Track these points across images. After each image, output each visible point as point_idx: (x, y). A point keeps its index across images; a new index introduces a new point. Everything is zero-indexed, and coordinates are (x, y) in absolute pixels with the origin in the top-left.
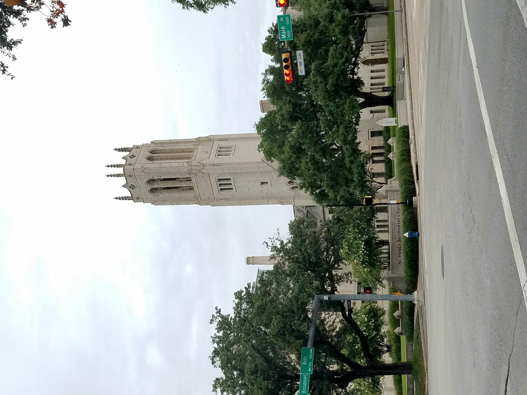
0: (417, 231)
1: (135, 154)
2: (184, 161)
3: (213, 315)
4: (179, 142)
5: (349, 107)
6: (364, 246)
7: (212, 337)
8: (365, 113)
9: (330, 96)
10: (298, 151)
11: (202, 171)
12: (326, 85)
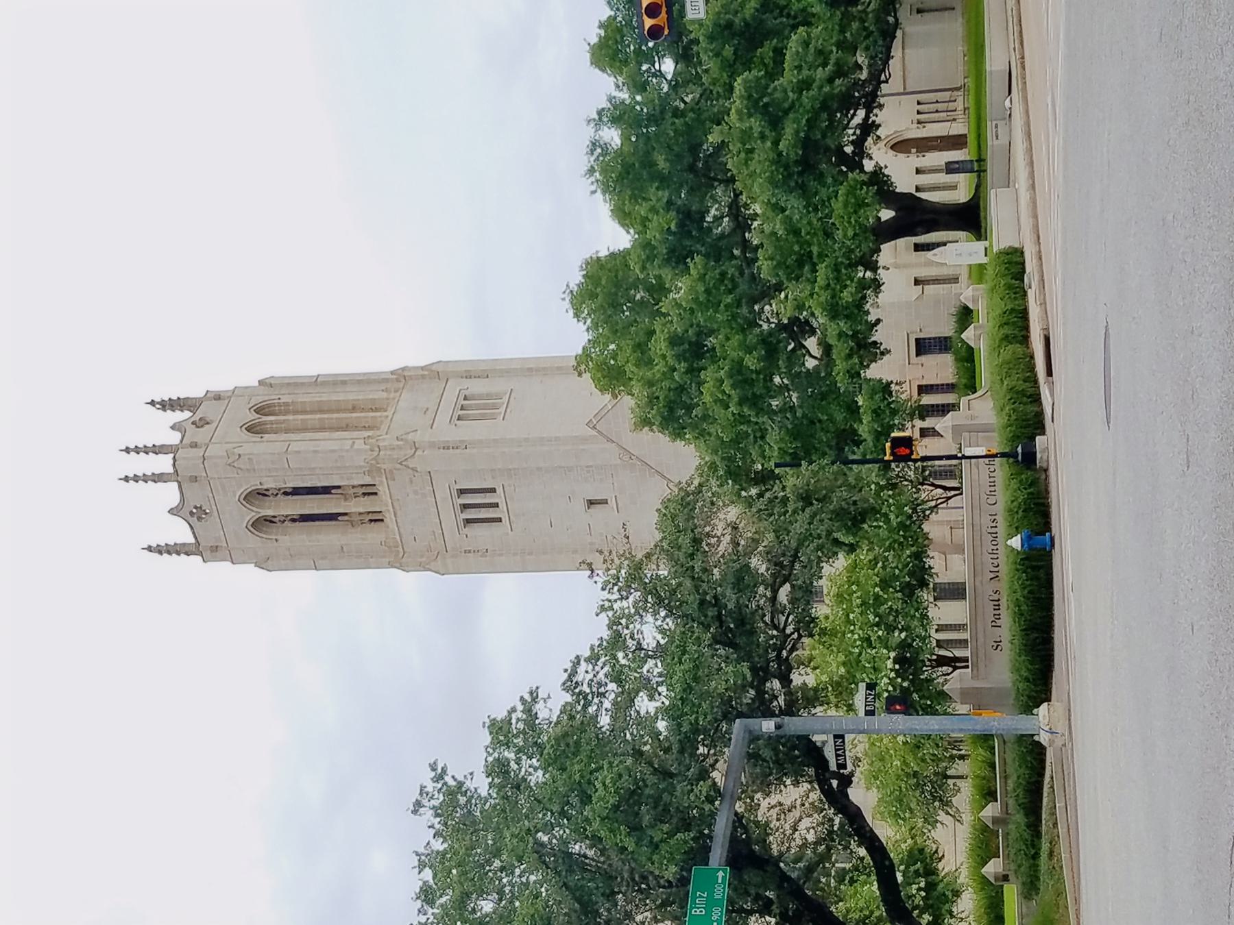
0: (1050, 530)
1: (210, 417)
2: (356, 434)
3: (422, 788)
4: (344, 383)
5: (846, 205)
6: (895, 662)
7: (417, 854)
8: (896, 259)
9: (790, 176)
10: (694, 351)
11: (411, 463)
12: (776, 143)
